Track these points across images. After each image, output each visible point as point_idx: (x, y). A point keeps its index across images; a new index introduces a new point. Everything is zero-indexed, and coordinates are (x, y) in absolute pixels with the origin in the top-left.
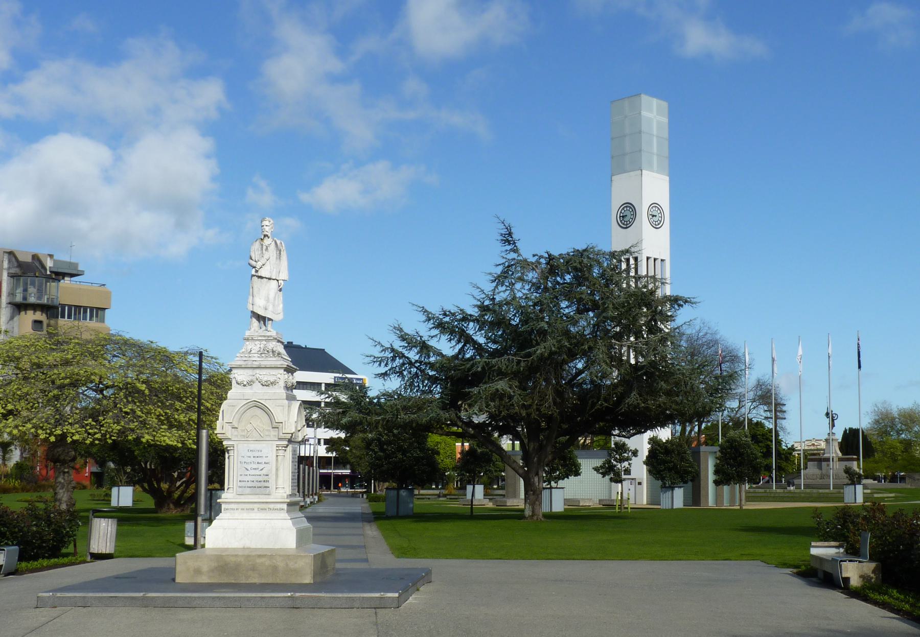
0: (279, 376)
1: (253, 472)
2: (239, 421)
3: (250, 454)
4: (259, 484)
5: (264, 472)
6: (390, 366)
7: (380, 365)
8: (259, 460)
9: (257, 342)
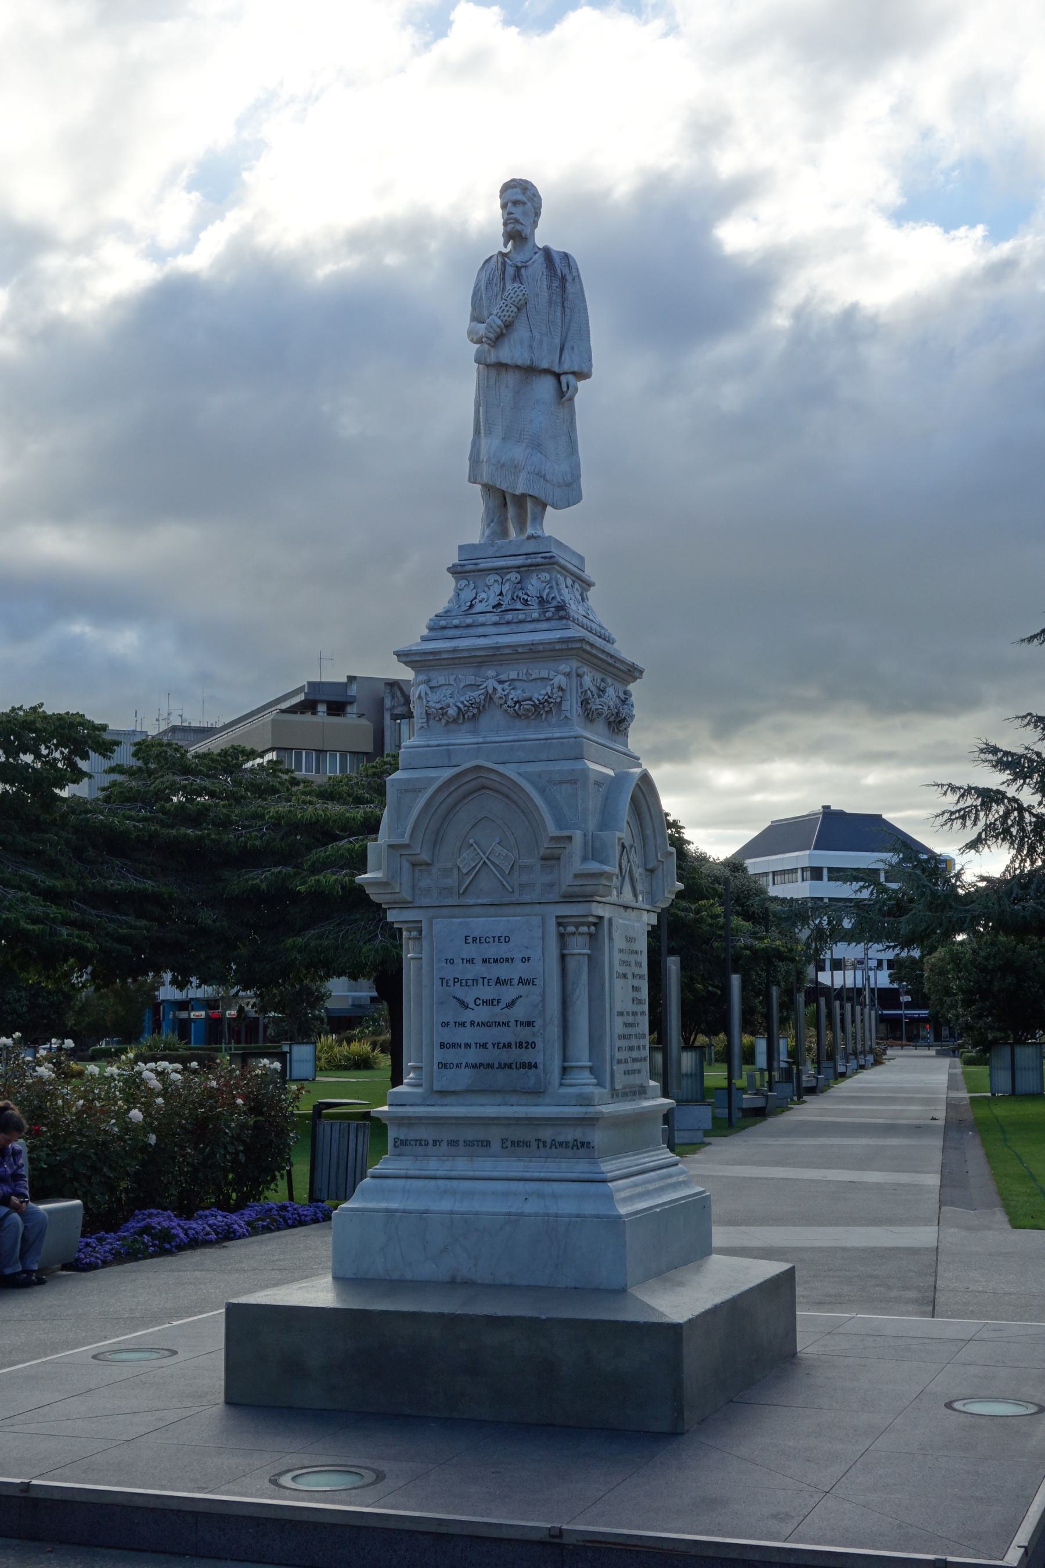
0: (560, 680)
1: (483, 1014)
2: (437, 841)
3: (470, 950)
4: (504, 1056)
5: (519, 1012)
6: (981, 824)
7: (964, 825)
8: (503, 971)
9: (491, 579)
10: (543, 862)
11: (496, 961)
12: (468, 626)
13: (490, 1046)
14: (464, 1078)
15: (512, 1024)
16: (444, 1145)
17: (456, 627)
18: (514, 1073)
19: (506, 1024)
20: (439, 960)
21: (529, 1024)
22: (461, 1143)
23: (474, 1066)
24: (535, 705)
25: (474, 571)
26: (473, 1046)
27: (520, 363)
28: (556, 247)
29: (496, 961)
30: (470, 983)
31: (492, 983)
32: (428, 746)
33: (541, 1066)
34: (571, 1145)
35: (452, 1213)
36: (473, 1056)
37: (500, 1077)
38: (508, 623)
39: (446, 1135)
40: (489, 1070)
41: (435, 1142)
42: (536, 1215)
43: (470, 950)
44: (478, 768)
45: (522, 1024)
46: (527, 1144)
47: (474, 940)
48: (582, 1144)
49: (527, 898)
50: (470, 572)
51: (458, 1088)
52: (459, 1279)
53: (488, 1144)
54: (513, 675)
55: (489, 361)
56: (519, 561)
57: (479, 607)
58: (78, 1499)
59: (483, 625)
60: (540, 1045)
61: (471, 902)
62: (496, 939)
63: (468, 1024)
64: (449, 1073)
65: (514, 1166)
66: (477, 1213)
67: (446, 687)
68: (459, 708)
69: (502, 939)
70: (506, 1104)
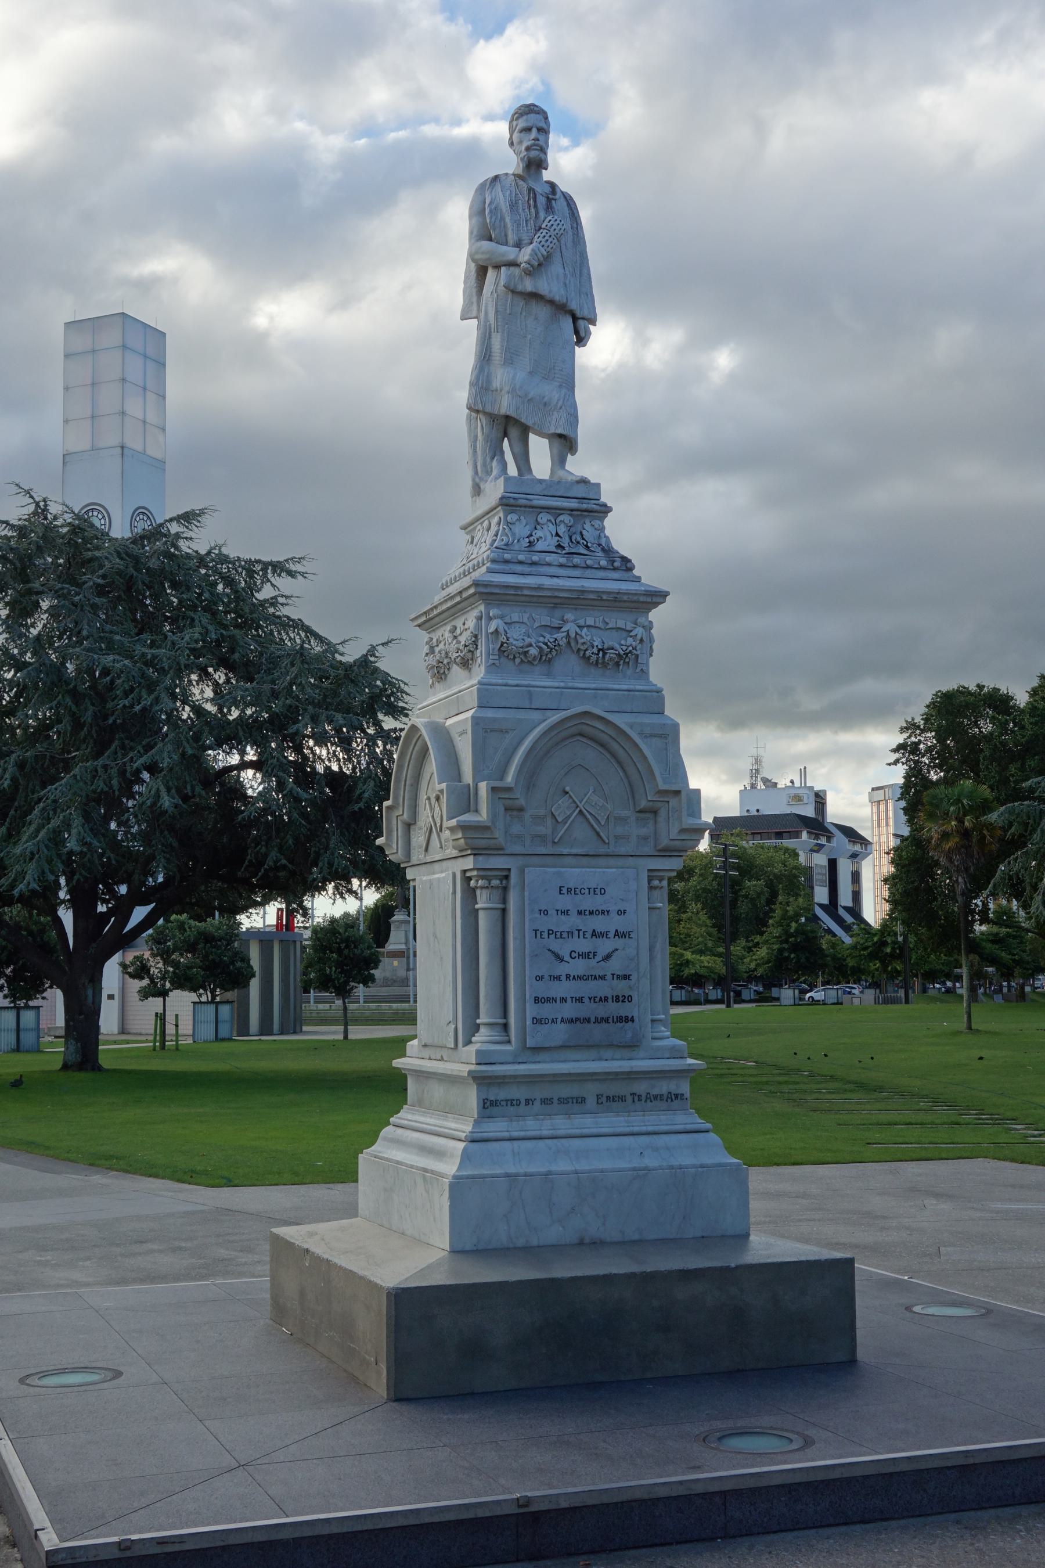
1: (579, 967)
3: (565, 902)
4: (601, 1010)
5: (615, 966)
8: (598, 923)
9: (543, 518)
10: (639, 815)
11: (591, 913)
12: (534, 564)
13: (586, 1000)
14: (559, 1033)
15: (609, 977)
16: (537, 1103)
17: (521, 563)
18: (611, 1027)
19: (603, 978)
20: (532, 911)
21: (626, 977)
22: (555, 1101)
23: (571, 1021)
24: (619, 655)
25: (525, 507)
26: (569, 1000)
27: (557, 298)
28: (563, 187)
29: (591, 913)
30: (565, 935)
31: (588, 935)
32: (506, 685)
33: (636, 1019)
34: (665, 1097)
35: (576, 1172)
36: (568, 1010)
37: (598, 1032)
38: (575, 566)
39: (539, 1093)
40: (586, 1025)
41: (527, 1102)
42: (661, 1168)
43: (565, 902)
44: (586, 713)
45: (618, 977)
46: (622, 1099)
47: (569, 890)
48: (676, 1096)
49: (622, 850)
50: (521, 506)
51: (553, 1044)
52: (587, 1240)
53: (583, 1100)
54: (590, 621)
55: (520, 288)
56: (573, 504)
57: (540, 546)
58: (590, 1502)
59: (549, 564)
60: (635, 999)
61: (565, 851)
62: (592, 891)
63: (563, 978)
64: (545, 1028)
65: (608, 1122)
66: (602, 1171)
67: (518, 625)
68: (540, 648)
69: (598, 891)
70: (600, 1059)
